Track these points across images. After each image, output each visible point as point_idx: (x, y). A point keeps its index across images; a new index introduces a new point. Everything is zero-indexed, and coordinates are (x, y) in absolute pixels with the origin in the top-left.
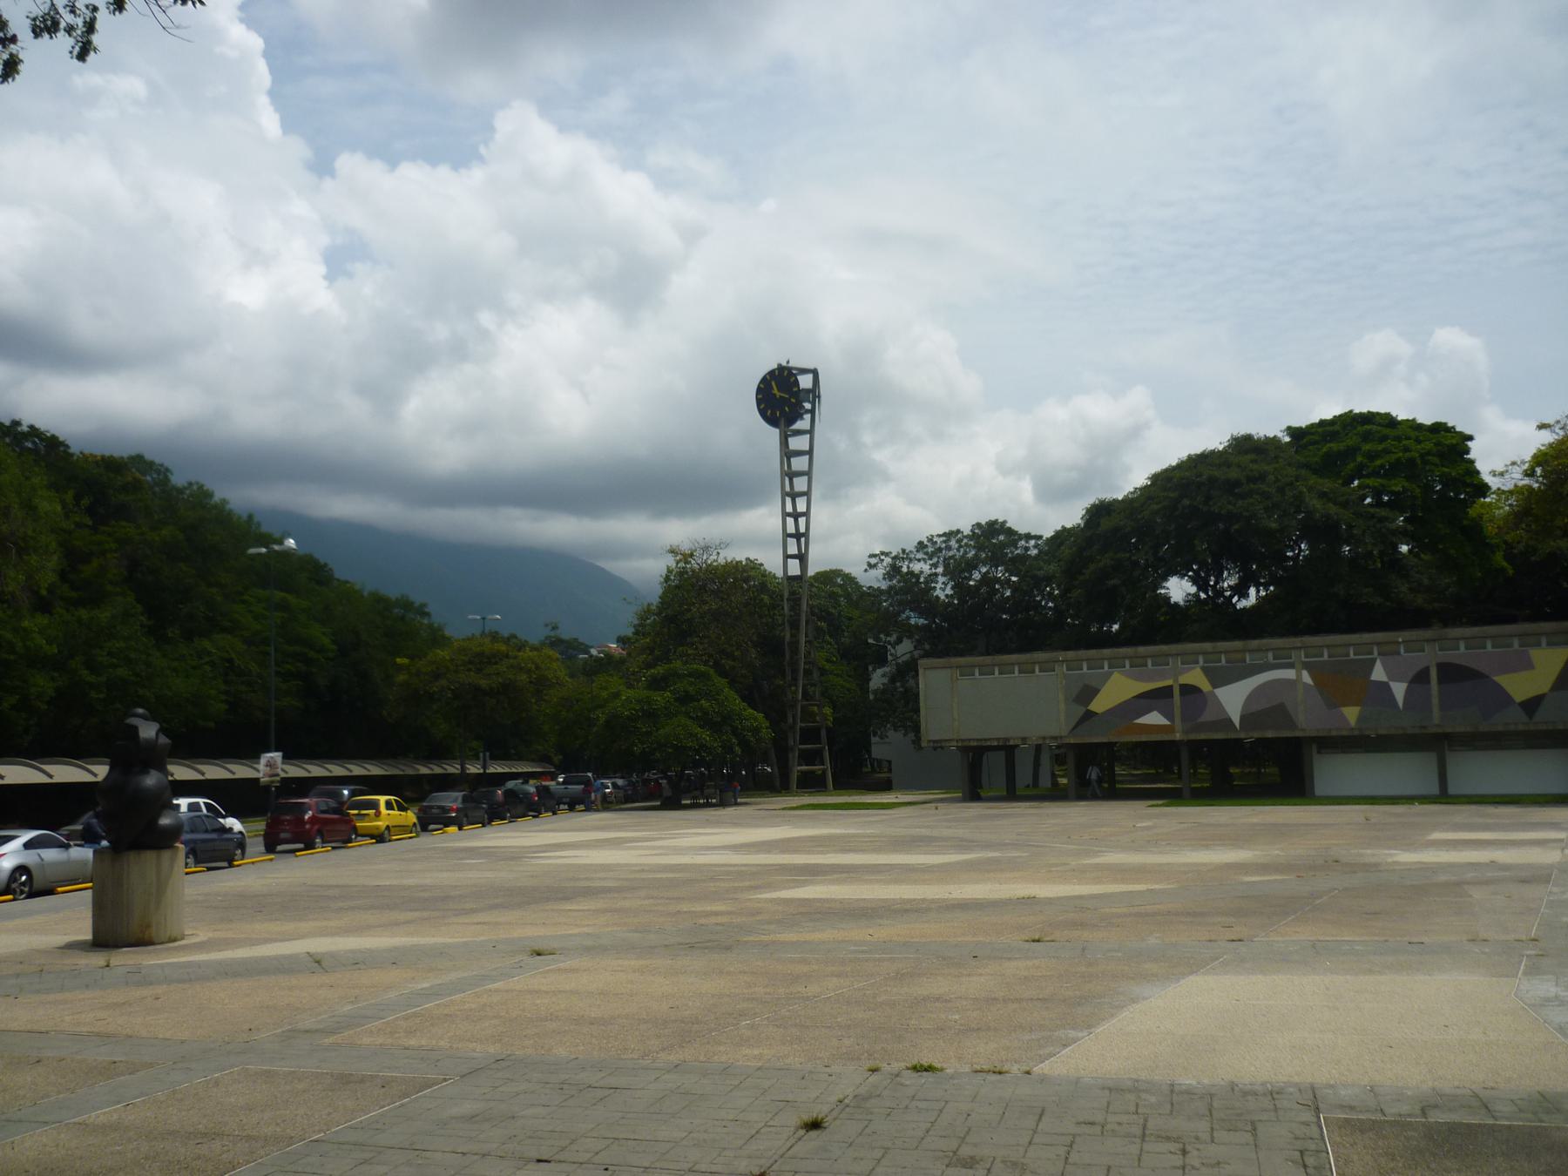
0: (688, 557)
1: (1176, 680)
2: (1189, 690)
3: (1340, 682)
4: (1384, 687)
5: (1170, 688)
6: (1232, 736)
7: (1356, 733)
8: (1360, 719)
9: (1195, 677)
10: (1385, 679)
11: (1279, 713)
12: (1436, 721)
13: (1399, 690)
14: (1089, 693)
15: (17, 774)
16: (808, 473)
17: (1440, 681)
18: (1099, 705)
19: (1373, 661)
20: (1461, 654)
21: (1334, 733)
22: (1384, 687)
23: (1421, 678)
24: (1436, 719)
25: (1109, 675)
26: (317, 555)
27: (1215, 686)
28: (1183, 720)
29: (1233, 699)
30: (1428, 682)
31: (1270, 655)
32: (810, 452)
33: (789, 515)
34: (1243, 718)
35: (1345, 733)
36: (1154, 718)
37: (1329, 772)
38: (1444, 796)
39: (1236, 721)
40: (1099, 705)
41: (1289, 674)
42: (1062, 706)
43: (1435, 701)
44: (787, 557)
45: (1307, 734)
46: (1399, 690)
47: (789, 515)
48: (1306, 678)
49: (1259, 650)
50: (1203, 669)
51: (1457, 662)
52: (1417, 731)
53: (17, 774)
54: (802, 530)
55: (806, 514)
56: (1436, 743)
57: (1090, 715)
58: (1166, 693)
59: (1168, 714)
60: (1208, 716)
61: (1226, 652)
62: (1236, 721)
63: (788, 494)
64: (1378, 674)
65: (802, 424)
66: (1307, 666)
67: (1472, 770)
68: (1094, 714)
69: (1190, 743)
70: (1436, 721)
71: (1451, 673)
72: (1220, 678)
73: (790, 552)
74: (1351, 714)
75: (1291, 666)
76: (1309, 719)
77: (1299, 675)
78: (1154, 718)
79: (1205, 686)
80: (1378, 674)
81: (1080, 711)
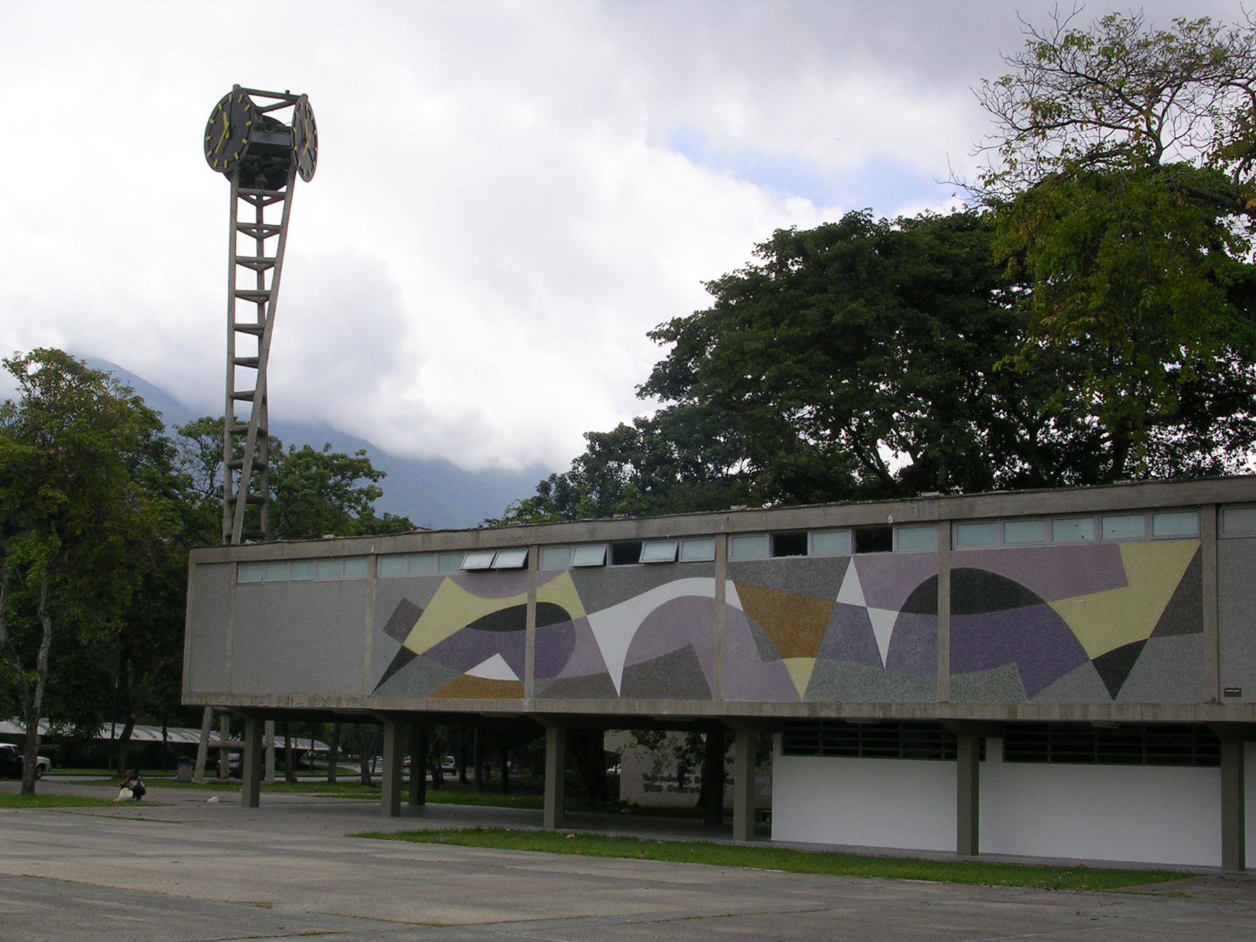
2: (551, 614)
4: (857, 620)
5: (522, 609)
13: (883, 623)
17: (956, 609)
18: (421, 639)
28: (538, 674)
34: (627, 672)
36: (495, 668)
46: (883, 623)
48: (732, 597)
54: (268, 286)
55: (275, 263)
57: (405, 657)
59: (517, 667)
60: (573, 669)
71: (981, 592)
74: (801, 670)
77: (720, 590)
78: (495, 668)
79: (572, 604)
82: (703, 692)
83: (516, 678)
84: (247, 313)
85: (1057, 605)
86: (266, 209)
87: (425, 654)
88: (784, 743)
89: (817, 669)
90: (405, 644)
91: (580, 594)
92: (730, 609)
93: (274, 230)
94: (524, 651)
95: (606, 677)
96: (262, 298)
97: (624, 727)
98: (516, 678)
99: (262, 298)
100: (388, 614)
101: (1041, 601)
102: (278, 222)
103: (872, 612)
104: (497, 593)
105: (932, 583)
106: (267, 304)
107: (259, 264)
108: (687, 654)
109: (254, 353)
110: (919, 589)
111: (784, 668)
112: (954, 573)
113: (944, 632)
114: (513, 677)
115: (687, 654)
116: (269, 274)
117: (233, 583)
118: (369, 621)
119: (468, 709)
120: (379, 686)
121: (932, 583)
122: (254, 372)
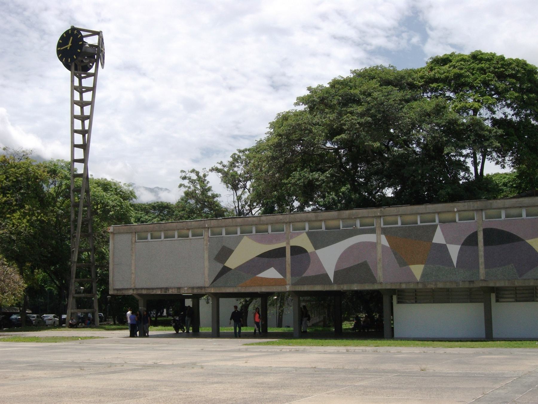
1: (288, 243)
2: (297, 251)
3: (410, 243)
4: (443, 248)
5: (284, 249)
6: (327, 288)
7: (420, 286)
9: (302, 240)
10: (445, 243)
11: (363, 270)
13: (454, 251)
14: (225, 253)
16: (93, 89)
17: (486, 243)
18: (233, 262)
19: (436, 226)
22: (443, 248)
23: (471, 241)
25: (241, 238)
27: (316, 247)
28: (293, 275)
29: (329, 259)
30: (477, 244)
31: (358, 223)
33: (77, 117)
34: (336, 273)
35: (412, 286)
36: (271, 273)
38: (488, 335)
39: (331, 277)
40: (233, 262)
41: (370, 238)
42: (207, 263)
43: (482, 260)
44: (74, 146)
45: (384, 287)
46: (454, 251)
47: (77, 117)
48: (384, 241)
49: (349, 218)
50: (308, 234)
51: (500, 228)
52: (467, 285)
54: (87, 128)
55: (90, 117)
56: (484, 295)
57: (226, 270)
58: (280, 253)
59: (282, 271)
60: (310, 272)
61: (325, 220)
62: (331, 277)
63: (77, 103)
64: (439, 238)
66: (384, 231)
67: (508, 313)
68: (229, 269)
71: (494, 237)
72: (321, 240)
73: (76, 143)
74: (417, 270)
75: (373, 231)
77: (379, 239)
78: (271, 273)
79: (308, 246)
80: (439, 238)
81: (219, 267)
82: (373, 280)
83: (281, 277)
84: (79, 139)
85: (530, 241)
86: (84, 94)
87: (236, 269)
88: (398, 298)
89: (425, 269)
90: (225, 265)
91: (312, 242)
92: (383, 246)
93: (87, 103)
94: (286, 266)
95: (326, 275)
96: (84, 132)
97: (189, 298)
98: (281, 277)
99: (84, 132)
100: (216, 252)
101: (523, 240)
102: (90, 99)
103: (448, 246)
104: (270, 242)
105: (475, 235)
106: (87, 135)
107: (83, 118)
108: (364, 265)
109: (82, 157)
110: (469, 236)
111: (410, 269)
112: (485, 231)
113: (481, 253)
114: (280, 276)
115: (364, 265)
116: (87, 122)
117: (133, 241)
118: (206, 256)
119: (253, 291)
120: (212, 283)
121: (475, 235)
122: (83, 165)
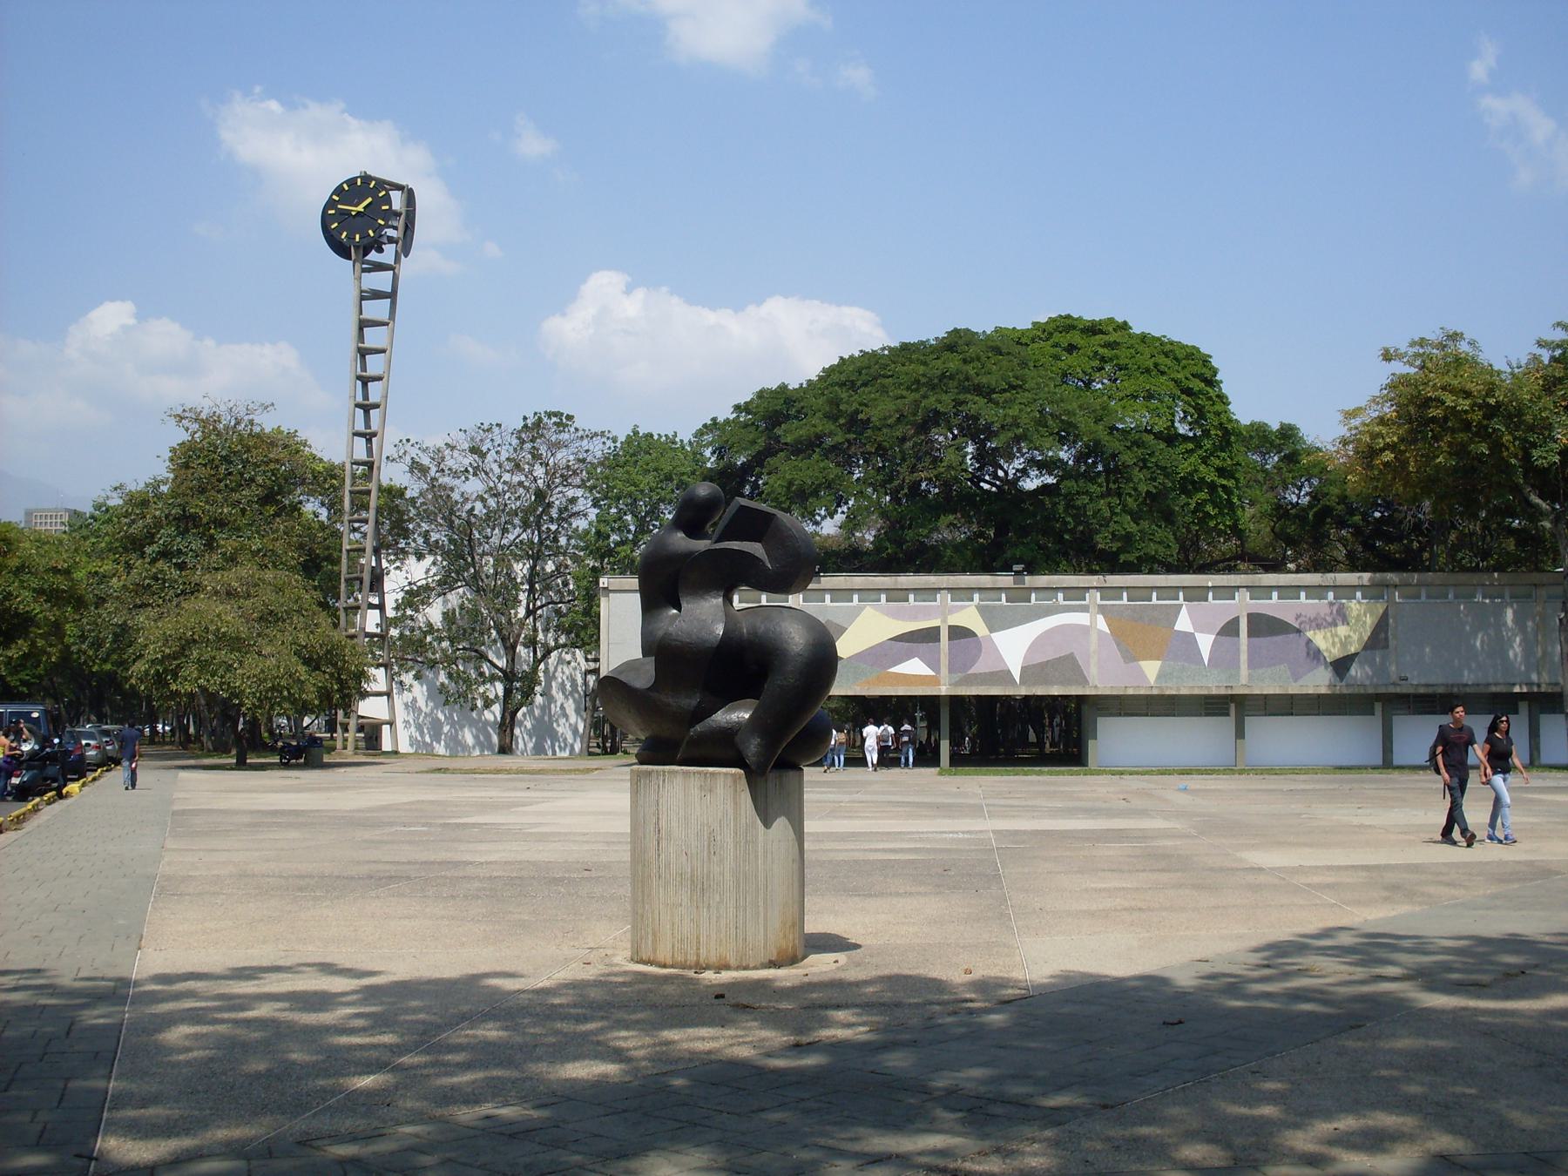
0: (208, 424)
1: (944, 621)
4: (1189, 639)
5: (938, 629)
8: (1161, 676)
9: (968, 615)
12: (1244, 680)
13: (1205, 642)
15: (1565, 1024)
20: (1273, 606)
21: (1130, 692)
22: (1189, 639)
24: (1245, 680)
26: (657, 426)
32: (392, 296)
34: (1024, 670)
37: (1111, 739)
41: (1082, 619)
43: (1244, 657)
46: (1205, 642)
48: (1102, 624)
50: (978, 607)
53: (1565, 1024)
58: (931, 635)
59: (933, 663)
60: (980, 667)
65: (388, 254)
66: (1102, 610)
69: (952, 698)
70: (1244, 680)
71: (1262, 626)
72: (996, 622)
75: (1085, 609)
76: (1102, 675)
78: (914, 667)
80: (1183, 623)
